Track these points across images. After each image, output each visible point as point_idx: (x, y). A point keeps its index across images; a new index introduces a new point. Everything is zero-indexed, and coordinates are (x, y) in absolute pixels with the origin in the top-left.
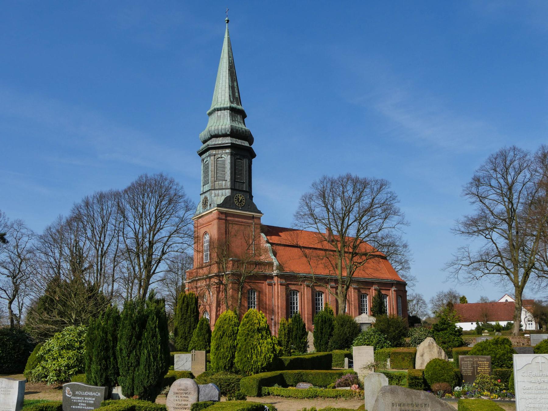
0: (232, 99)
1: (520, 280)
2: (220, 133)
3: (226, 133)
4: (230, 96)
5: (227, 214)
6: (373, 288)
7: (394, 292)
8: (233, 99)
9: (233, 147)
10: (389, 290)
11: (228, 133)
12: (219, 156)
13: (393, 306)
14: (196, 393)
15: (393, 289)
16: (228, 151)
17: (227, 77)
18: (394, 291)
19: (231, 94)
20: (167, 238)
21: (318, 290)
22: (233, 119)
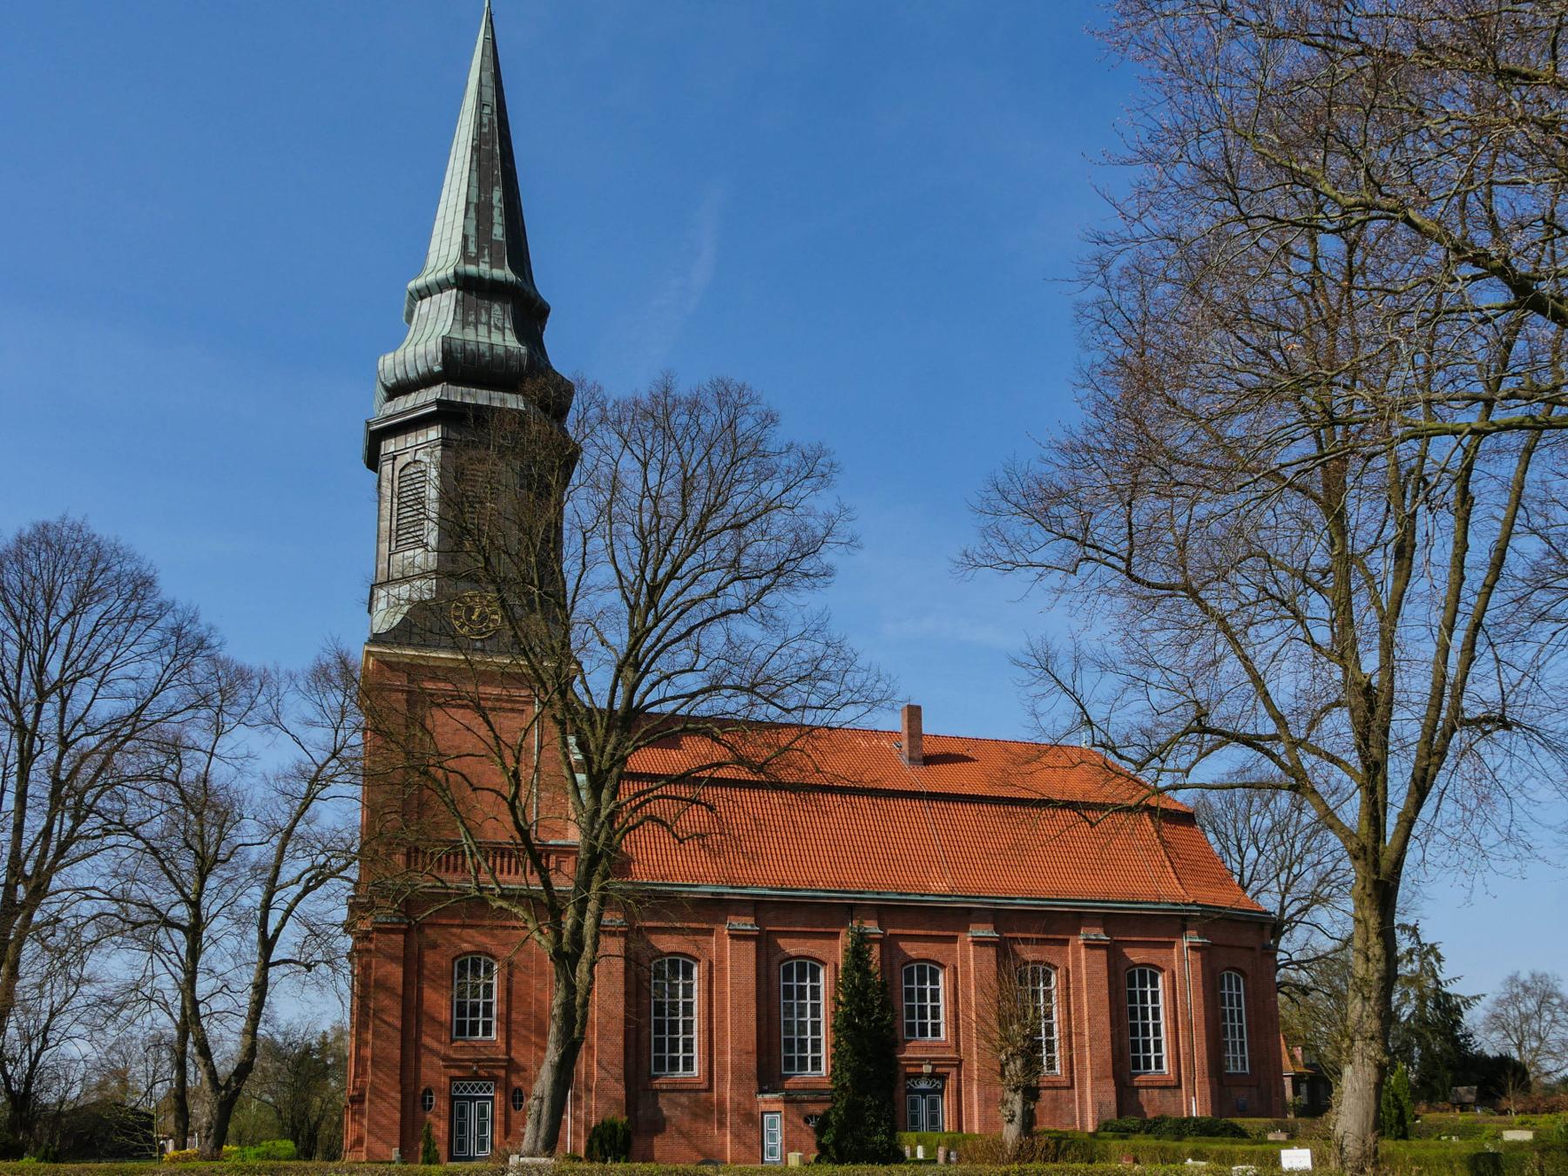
0: (472, 249)
1: (495, 201)
2: (412, 375)
3: (430, 371)
4: (465, 237)
5: (412, 670)
6: (1081, 940)
7: (1189, 955)
8: (480, 248)
9: (446, 414)
10: (1170, 945)
11: (437, 368)
12: (408, 458)
13: (1186, 1013)
14: (515, 987)
15: (1191, 938)
16: (434, 433)
17: (466, 174)
18: (1192, 948)
19: (472, 231)
20: (710, 526)
21: (792, 951)
22: (465, 315)
